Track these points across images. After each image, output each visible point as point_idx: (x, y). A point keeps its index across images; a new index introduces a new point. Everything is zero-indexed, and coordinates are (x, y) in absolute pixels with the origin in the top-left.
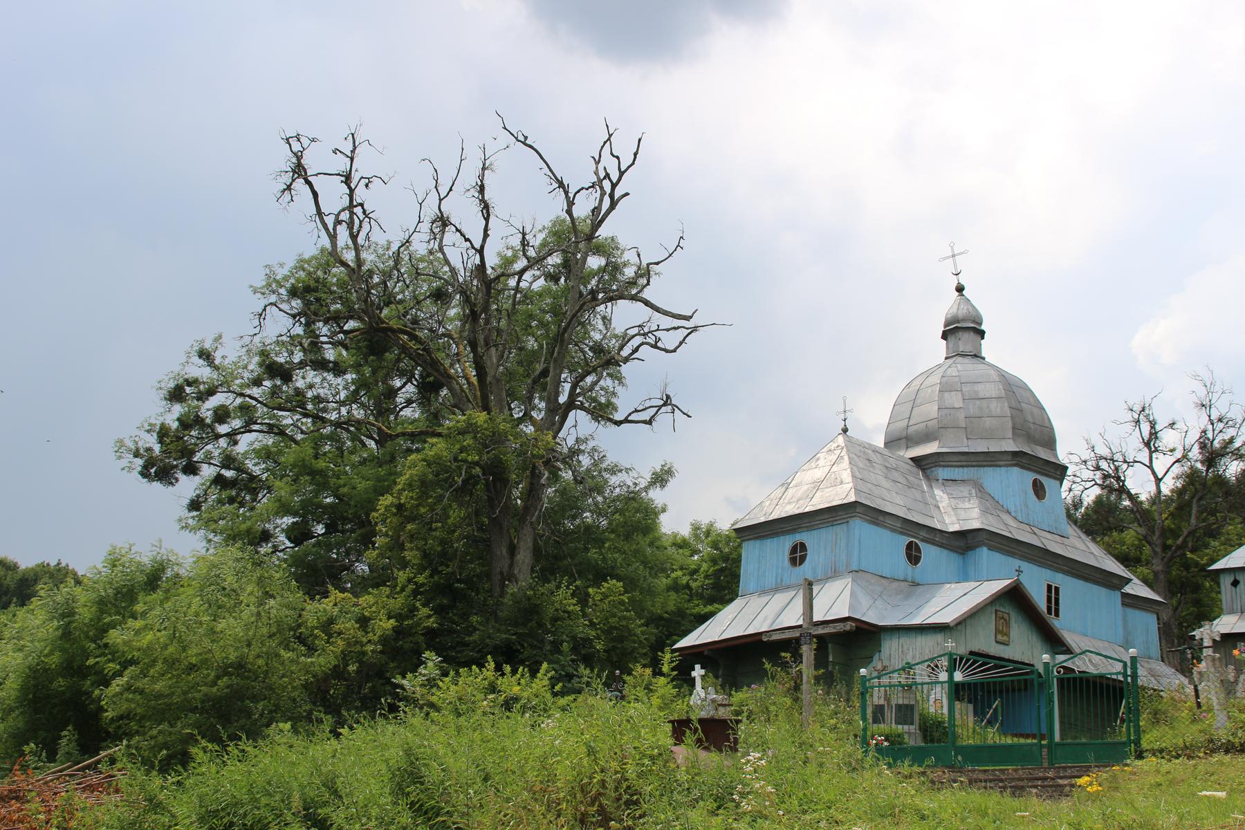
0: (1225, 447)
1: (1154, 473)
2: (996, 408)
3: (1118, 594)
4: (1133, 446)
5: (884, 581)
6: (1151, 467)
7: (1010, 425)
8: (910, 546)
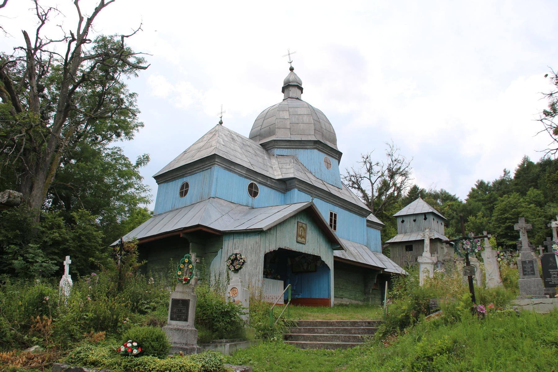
0: (397, 171)
1: (371, 181)
2: (306, 119)
3: (365, 219)
4: (363, 172)
5: (232, 205)
6: (370, 179)
7: (313, 128)
8: (251, 186)
